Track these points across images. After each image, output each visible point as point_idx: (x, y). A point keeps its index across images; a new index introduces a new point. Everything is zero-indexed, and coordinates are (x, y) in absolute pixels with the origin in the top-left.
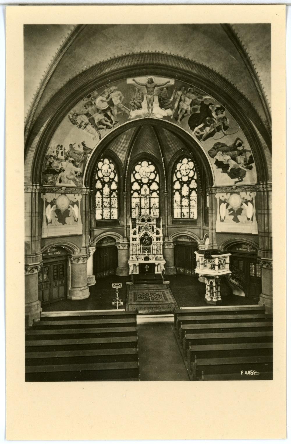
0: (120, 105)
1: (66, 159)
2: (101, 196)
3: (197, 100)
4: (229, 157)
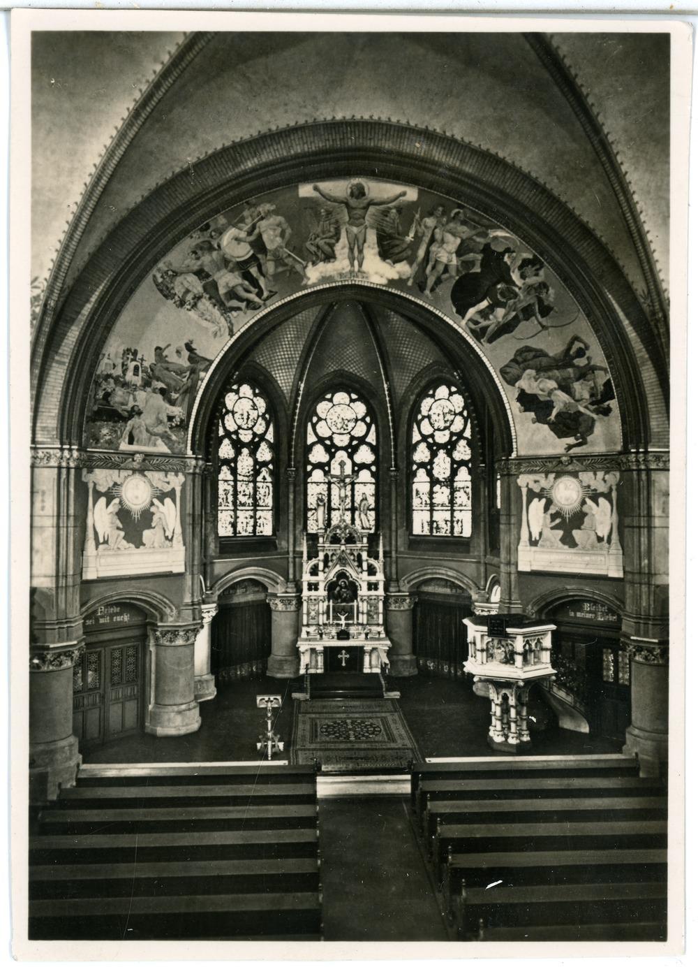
1: (146, 384)
2: (231, 478)
3: (474, 241)
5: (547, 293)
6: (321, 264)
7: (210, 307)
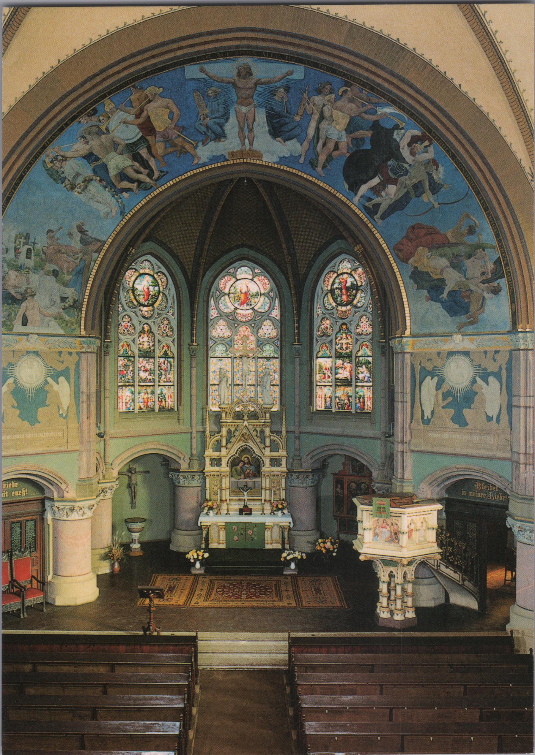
0: (170, 132)
1: (39, 267)
3: (362, 118)
4: (444, 262)
5: (437, 170)
6: (212, 143)
7: (102, 188)
